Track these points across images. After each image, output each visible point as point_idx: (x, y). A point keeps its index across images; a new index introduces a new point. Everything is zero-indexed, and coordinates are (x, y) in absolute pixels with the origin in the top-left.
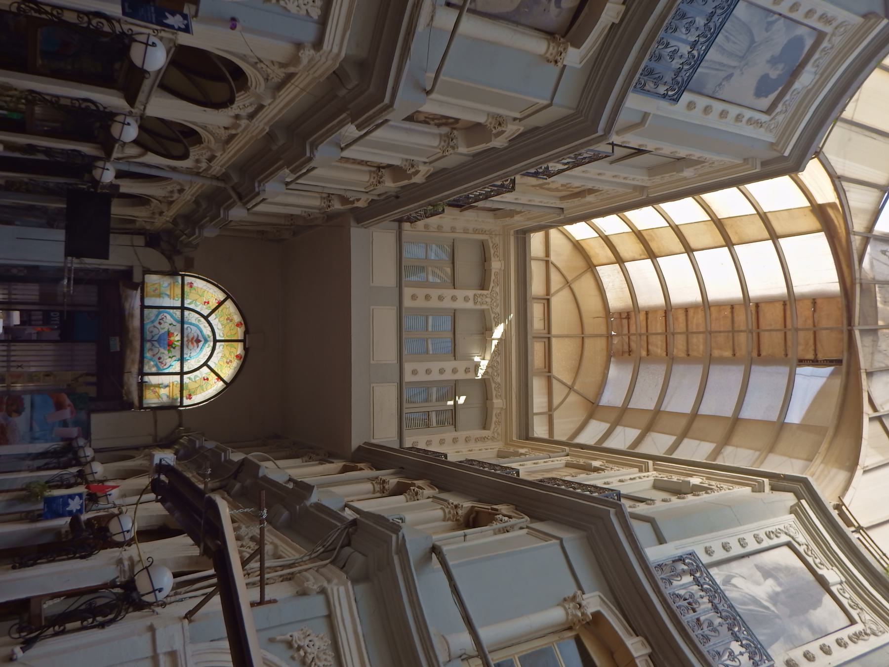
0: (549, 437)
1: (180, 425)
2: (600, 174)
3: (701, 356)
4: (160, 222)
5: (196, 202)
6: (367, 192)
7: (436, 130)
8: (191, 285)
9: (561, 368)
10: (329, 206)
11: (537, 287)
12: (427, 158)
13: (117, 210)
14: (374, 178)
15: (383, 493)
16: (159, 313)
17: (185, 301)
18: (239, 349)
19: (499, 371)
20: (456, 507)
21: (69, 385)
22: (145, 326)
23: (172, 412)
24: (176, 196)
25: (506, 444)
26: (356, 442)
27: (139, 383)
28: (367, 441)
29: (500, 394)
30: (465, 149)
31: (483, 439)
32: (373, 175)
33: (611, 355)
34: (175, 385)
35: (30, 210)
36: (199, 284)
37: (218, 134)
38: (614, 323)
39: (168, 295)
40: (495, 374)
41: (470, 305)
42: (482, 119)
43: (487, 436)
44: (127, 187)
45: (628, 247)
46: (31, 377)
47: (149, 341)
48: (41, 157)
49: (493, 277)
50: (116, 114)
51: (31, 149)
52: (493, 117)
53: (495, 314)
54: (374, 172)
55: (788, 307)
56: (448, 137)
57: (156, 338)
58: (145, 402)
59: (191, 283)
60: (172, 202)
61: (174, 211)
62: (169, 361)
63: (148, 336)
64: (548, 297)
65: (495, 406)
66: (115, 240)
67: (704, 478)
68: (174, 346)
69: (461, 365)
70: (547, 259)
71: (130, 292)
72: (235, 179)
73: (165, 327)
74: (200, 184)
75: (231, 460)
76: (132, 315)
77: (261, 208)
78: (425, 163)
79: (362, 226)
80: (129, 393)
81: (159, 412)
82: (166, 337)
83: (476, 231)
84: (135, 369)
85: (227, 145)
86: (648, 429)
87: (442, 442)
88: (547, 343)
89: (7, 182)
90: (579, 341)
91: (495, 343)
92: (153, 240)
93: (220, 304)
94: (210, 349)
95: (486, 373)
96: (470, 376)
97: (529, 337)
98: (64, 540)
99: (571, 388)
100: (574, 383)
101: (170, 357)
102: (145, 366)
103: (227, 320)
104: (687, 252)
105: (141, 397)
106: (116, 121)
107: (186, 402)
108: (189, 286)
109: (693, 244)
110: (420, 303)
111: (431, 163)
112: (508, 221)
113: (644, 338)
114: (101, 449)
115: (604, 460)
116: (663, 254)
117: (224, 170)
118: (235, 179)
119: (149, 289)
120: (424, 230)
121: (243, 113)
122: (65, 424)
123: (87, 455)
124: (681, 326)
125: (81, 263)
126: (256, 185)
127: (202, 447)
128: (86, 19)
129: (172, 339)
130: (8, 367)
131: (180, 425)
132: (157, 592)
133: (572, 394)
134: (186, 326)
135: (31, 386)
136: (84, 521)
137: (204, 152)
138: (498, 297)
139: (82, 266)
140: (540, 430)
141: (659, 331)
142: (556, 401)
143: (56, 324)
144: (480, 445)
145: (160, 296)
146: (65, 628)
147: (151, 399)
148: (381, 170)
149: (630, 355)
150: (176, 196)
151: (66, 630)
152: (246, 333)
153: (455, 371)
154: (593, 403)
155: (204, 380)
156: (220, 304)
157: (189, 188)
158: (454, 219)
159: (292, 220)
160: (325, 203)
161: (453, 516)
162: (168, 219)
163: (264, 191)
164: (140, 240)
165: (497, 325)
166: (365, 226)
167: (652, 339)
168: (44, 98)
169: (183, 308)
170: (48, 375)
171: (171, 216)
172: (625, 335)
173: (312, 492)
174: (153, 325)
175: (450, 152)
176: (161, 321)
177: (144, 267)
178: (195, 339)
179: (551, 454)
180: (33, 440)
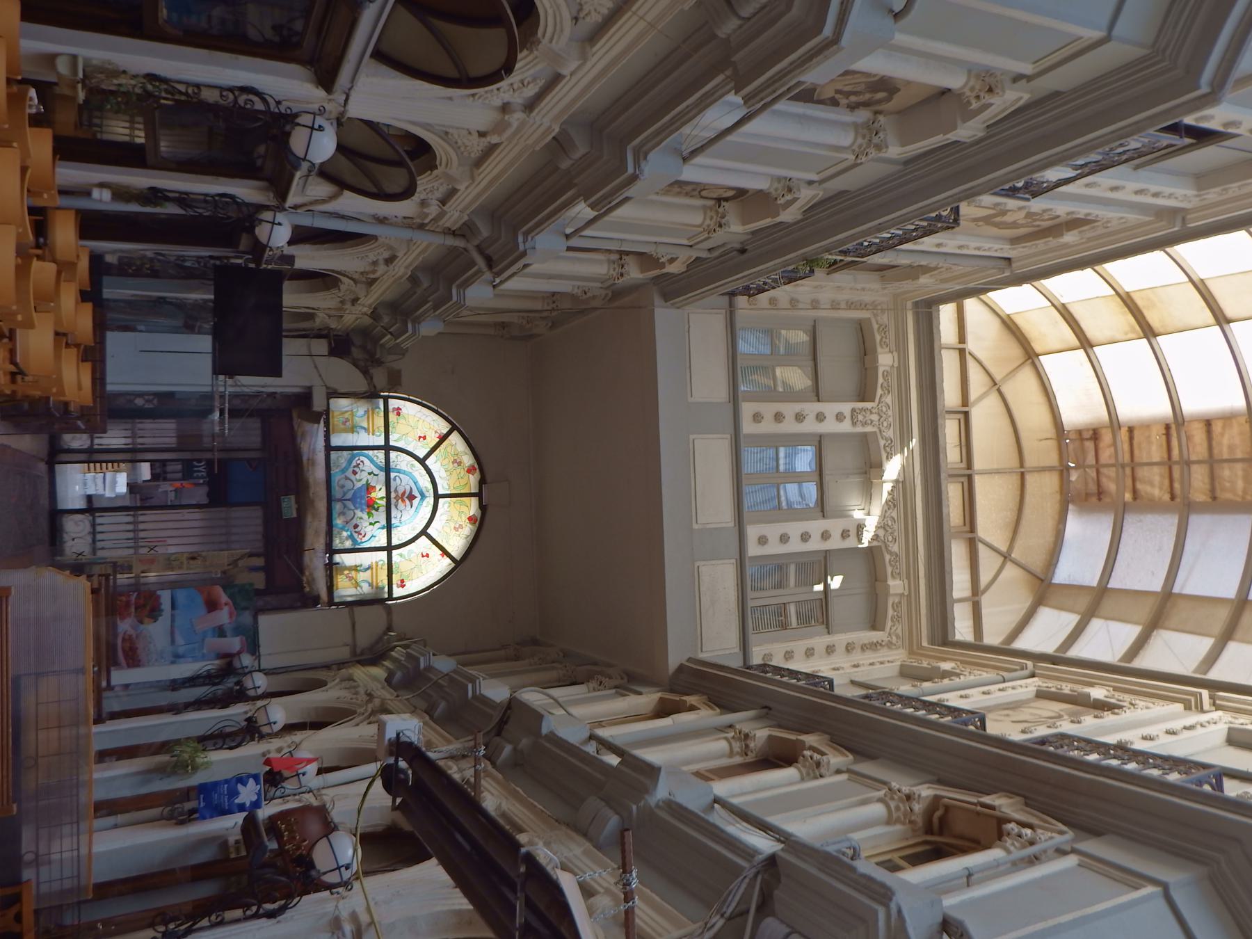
0: (975, 640)
1: (389, 629)
2: (1115, 189)
3: (1239, 499)
4: (354, 317)
5: (413, 279)
6: (691, 246)
7: (848, 117)
8: (398, 411)
9: (990, 526)
10: (622, 275)
11: (950, 395)
12: (818, 174)
13: (293, 298)
14: (711, 218)
15: (747, 755)
16: (353, 457)
17: (390, 437)
18: (472, 506)
19: (896, 534)
20: (909, 797)
21: (224, 572)
22: (332, 479)
23: (377, 609)
24: (382, 268)
25: (911, 652)
26: (675, 659)
27: (326, 565)
28: (692, 656)
29: (898, 571)
31: (874, 646)
32: (709, 214)
33: (1068, 499)
34: (380, 566)
35: (158, 304)
36: (409, 409)
37: (466, 147)
38: (1071, 447)
39: (364, 428)
40: (890, 538)
41: (846, 427)
42: (954, 81)
43: (880, 642)
44: (309, 258)
45: (1116, 320)
46: (170, 563)
47: (339, 500)
48: (172, 209)
49: (881, 380)
50: (296, 115)
51: (155, 196)
52: (978, 76)
53: (886, 439)
54: (711, 208)
56: (869, 128)
57: (349, 496)
58: (336, 594)
59: (399, 409)
60: (375, 280)
61: (376, 296)
62: (369, 530)
63: (337, 492)
64: (966, 409)
65: (892, 591)
66: (291, 347)
68: (376, 506)
69: (835, 526)
70: (961, 346)
71: (308, 426)
72: (485, 231)
73: (363, 477)
74: (425, 244)
75: (484, 696)
76: (312, 462)
77: (516, 284)
78: (810, 183)
79: (673, 304)
80: (312, 581)
81: (358, 610)
82: (364, 493)
83: (851, 306)
84: (320, 544)
85: (478, 169)
86: (1153, 625)
87: (809, 653)
88: (966, 485)
89: (120, 259)
90: (1015, 479)
91: (887, 487)
92: (340, 345)
93: (443, 438)
94: (430, 508)
95: (876, 537)
96: (851, 543)
97: (943, 476)
98: (233, 856)
99: (1006, 557)
100: (1011, 547)
101: (371, 524)
102: (334, 538)
103: (453, 463)
104: (1219, 323)
105: (331, 588)
106: (299, 124)
107: (397, 592)
108: (395, 412)
109: (1230, 312)
110: (767, 427)
111: (821, 182)
112: (907, 285)
113: (1128, 471)
114: (275, 669)
115: (1109, 686)
116: (1169, 331)
117: (466, 218)
118: (485, 231)
119: (336, 420)
120: (769, 307)
121: (518, 99)
122: (220, 632)
123: (257, 685)
124: (1199, 448)
125: (236, 385)
126: (520, 239)
127: (429, 668)
128: (231, 96)
129: (373, 495)
130: (136, 548)
131: (389, 629)
133: (1009, 565)
134: (393, 475)
135: (171, 575)
136: (263, 820)
137: (436, 184)
138: (890, 413)
139: (238, 389)
140: (962, 629)
141: (1156, 459)
142: (984, 578)
143: (202, 477)
144: (870, 656)
145: (353, 429)
146: (223, 919)
147: (346, 589)
148: (723, 203)
149: (1100, 499)
150: (382, 268)
152: (482, 482)
153: (825, 536)
154: (1042, 580)
155: (423, 556)
156: (443, 438)
157: (405, 254)
158: (816, 287)
159: (554, 302)
160: (614, 270)
161: (905, 815)
162: (365, 309)
163: (534, 248)
164: (321, 346)
165: (889, 457)
166: (677, 305)
167: (1142, 473)
168: (173, 87)
169: (387, 448)
170: (193, 558)
171: (370, 306)
172: (1090, 467)
173: (658, 779)
174: (343, 476)
175: (870, 156)
176: (356, 469)
177: (327, 388)
178: (406, 495)
179: (1005, 674)
180: (177, 657)
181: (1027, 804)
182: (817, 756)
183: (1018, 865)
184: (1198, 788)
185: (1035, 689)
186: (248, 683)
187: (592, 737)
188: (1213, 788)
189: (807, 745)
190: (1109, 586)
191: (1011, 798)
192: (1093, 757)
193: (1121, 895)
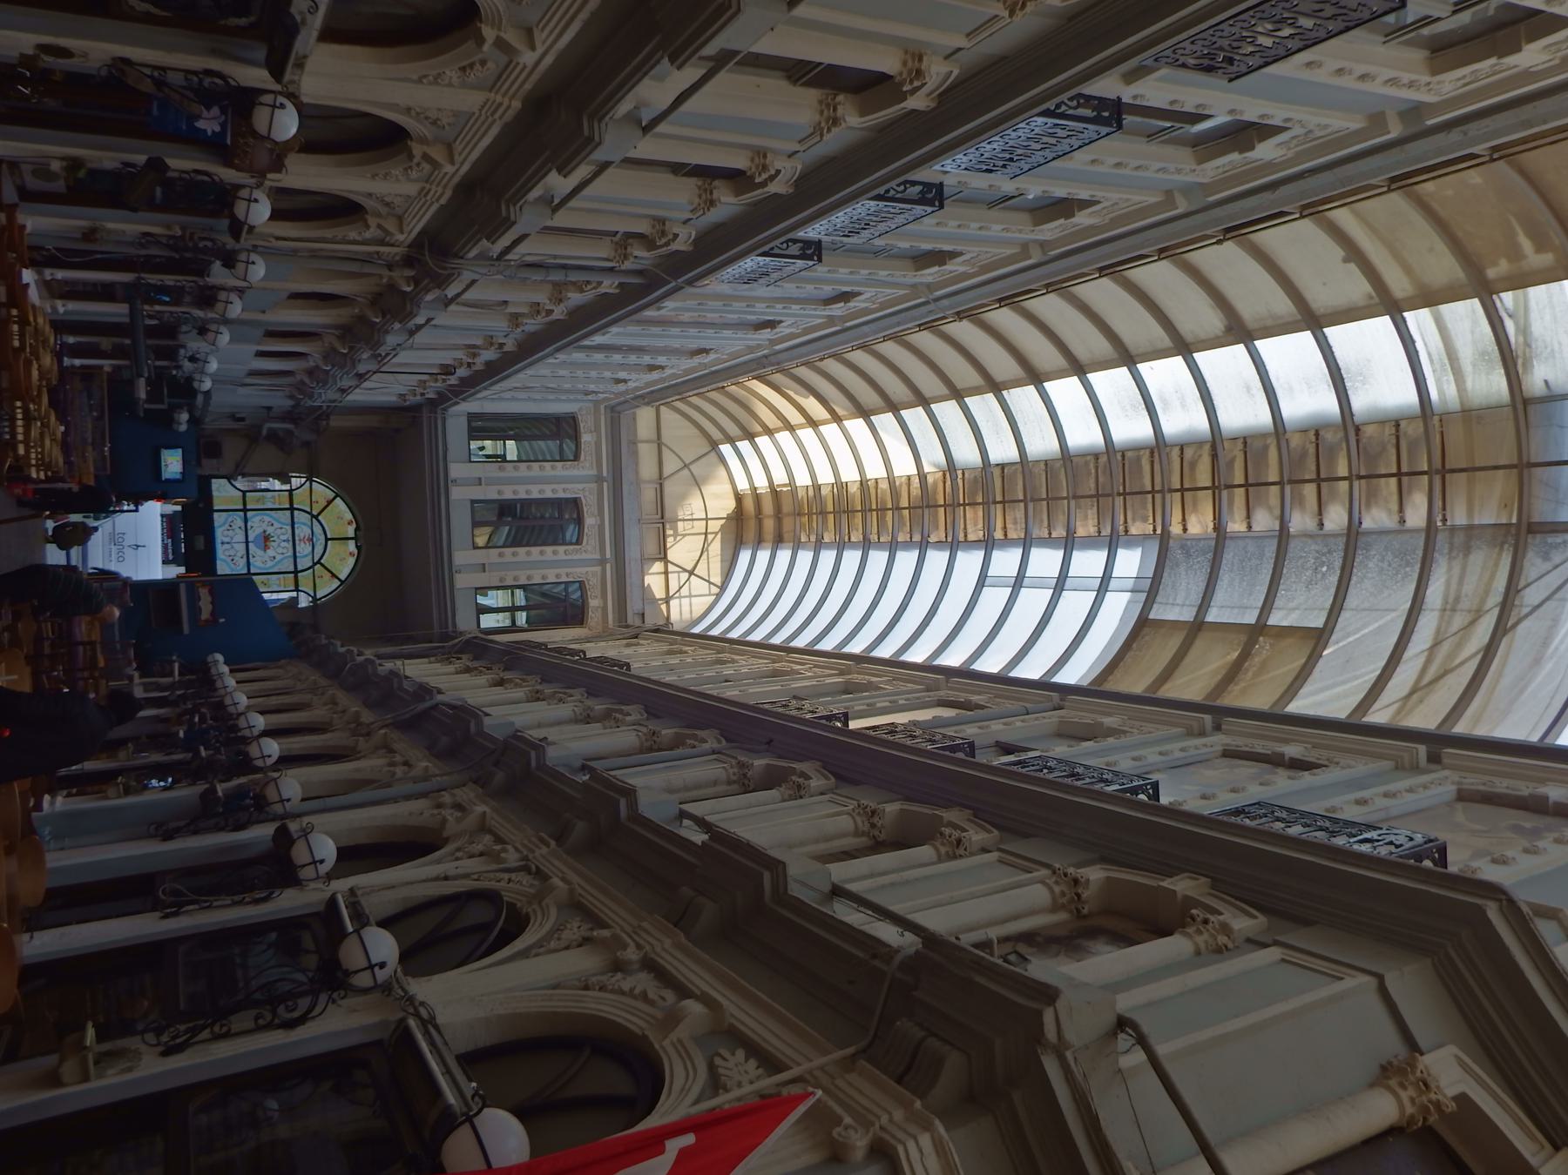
67: (1309, 746)
93: (330, 502)
106: (261, 104)
128: (195, 79)
132: (376, 969)
182: (956, 834)
183: (1199, 957)
184: (828, 723)
186: (253, 751)
187: (683, 815)
188: (1435, 865)
189: (945, 821)
190: (1151, 617)
192: (1295, 830)
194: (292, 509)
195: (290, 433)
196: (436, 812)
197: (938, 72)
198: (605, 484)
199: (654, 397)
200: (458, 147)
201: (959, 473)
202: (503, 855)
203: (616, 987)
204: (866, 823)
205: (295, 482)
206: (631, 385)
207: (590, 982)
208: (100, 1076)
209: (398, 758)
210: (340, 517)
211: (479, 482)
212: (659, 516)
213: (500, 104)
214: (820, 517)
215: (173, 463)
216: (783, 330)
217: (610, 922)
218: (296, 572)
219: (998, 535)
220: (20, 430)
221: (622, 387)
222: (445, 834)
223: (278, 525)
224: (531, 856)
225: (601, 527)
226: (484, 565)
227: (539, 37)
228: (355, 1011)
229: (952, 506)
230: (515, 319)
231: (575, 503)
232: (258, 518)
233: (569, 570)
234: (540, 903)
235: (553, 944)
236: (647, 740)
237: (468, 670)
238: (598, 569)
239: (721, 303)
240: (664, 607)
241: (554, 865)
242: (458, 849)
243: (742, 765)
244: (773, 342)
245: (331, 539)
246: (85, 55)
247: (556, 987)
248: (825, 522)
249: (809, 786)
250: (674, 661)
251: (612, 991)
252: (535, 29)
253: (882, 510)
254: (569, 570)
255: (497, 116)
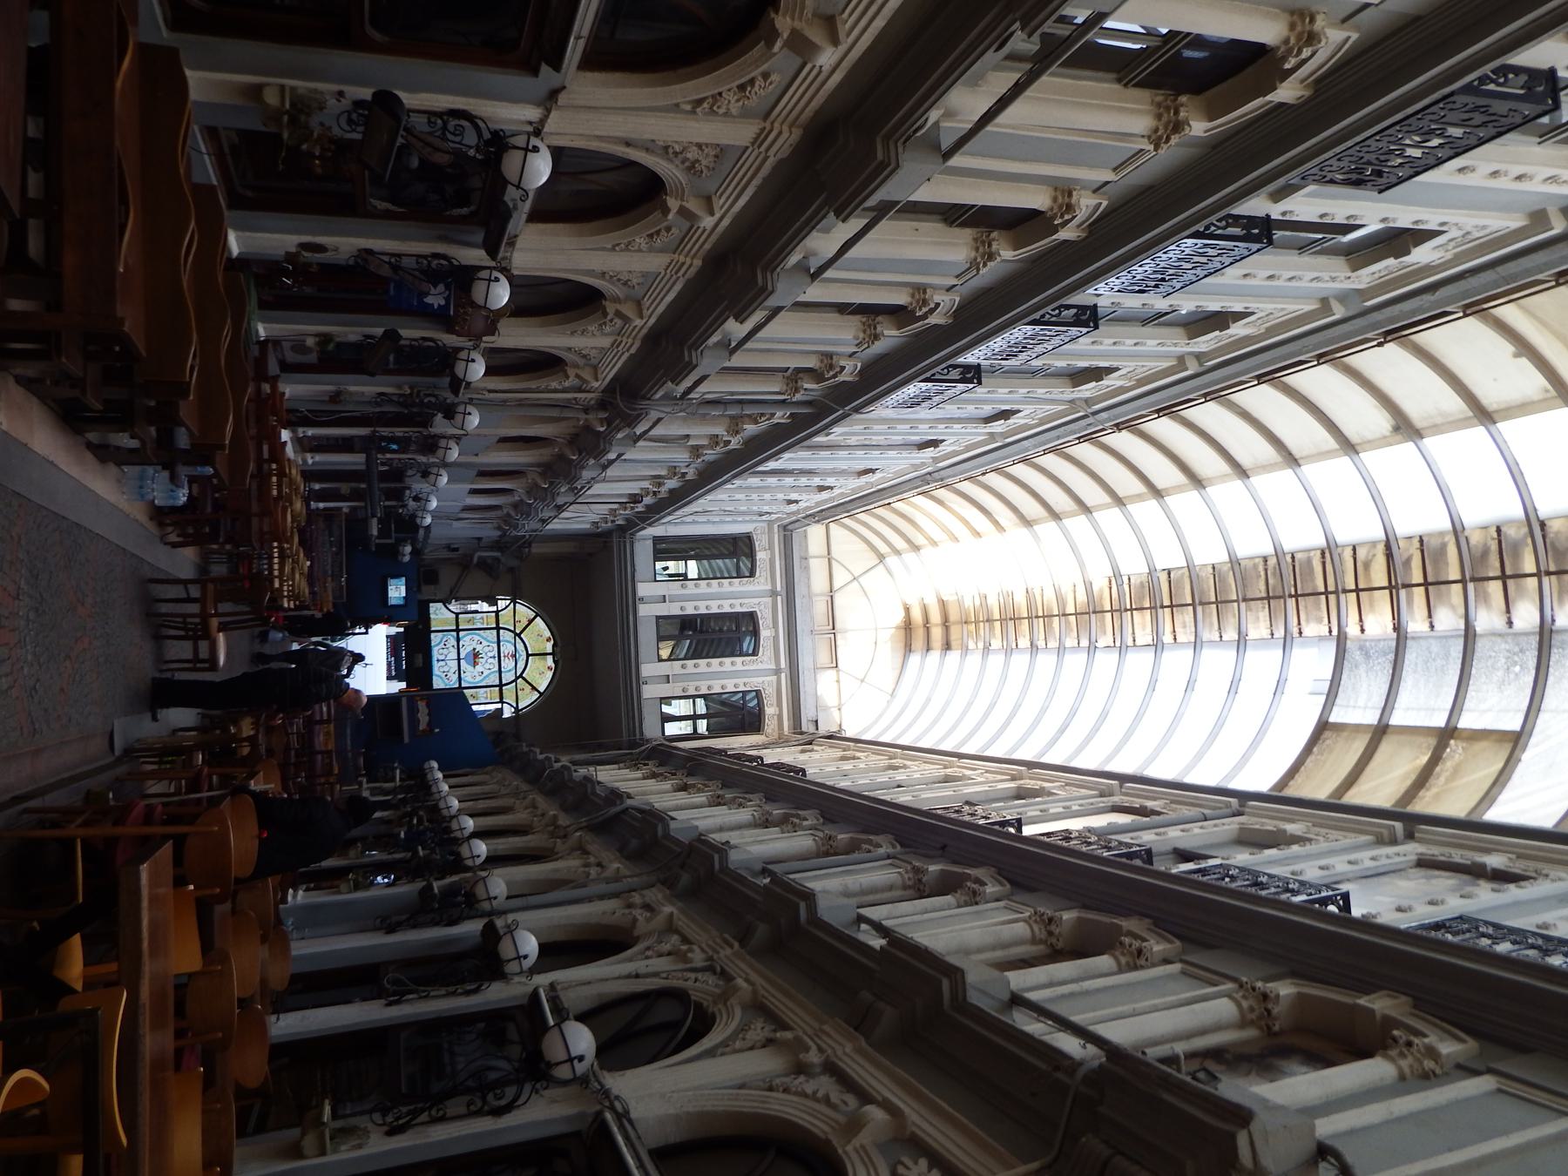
30: (1007, 255)
55: (1327, 555)
93: (530, 622)
113: (1197, 601)
123: (492, 895)
128: (425, 262)
146: (445, 1114)
151: (448, 1115)
181: (1156, 925)
182: (1136, 944)
183: (1403, 1084)
185: (1238, 826)
187: (861, 919)
189: (1124, 930)
191: (1396, 998)
192: (1503, 947)
193: (1532, 1125)
194: (498, 628)
195: (497, 559)
196: (627, 911)
197: (1087, 204)
198: (779, 598)
199: (822, 515)
200: (646, 302)
201: (1125, 579)
202: (689, 955)
203: (799, 1089)
204: (1043, 930)
205: (502, 604)
206: (802, 505)
207: (774, 1083)
208: (335, 1151)
209: (592, 860)
210: (540, 634)
211: (664, 599)
212: (831, 627)
213: (683, 264)
214: (987, 624)
215: (397, 591)
216: (944, 449)
217: (792, 1024)
218: (501, 686)
219: (1168, 638)
220: (276, 567)
221: (793, 507)
222: (636, 933)
223: (483, 643)
224: (715, 957)
225: (776, 638)
226: (668, 676)
227: (718, 203)
228: (556, 1101)
229: (1118, 611)
230: (696, 451)
231: (751, 617)
232: (470, 637)
233: (746, 680)
234: (725, 1004)
235: (738, 1044)
236: (823, 845)
237: (654, 776)
238: (774, 678)
239: (887, 427)
240: (836, 713)
241: (736, 965)
242: (648, 948)
243: (916, 870)
244: (936, 460)
245: (532, 655)
246: (336, 249)
247: (742, 1086)
248: (992, 629)
249: (985, 892)
250: (847, 766)
251: (796, 1094)
252: (713, 197)
253: (1048, 617)
254: (746, 680)
255: (680, 274)
